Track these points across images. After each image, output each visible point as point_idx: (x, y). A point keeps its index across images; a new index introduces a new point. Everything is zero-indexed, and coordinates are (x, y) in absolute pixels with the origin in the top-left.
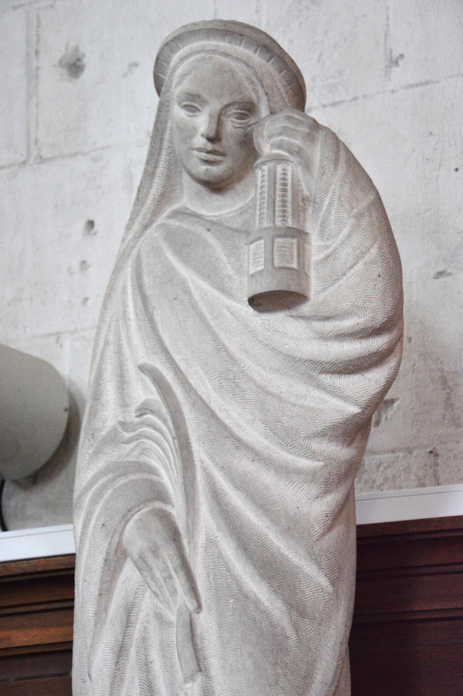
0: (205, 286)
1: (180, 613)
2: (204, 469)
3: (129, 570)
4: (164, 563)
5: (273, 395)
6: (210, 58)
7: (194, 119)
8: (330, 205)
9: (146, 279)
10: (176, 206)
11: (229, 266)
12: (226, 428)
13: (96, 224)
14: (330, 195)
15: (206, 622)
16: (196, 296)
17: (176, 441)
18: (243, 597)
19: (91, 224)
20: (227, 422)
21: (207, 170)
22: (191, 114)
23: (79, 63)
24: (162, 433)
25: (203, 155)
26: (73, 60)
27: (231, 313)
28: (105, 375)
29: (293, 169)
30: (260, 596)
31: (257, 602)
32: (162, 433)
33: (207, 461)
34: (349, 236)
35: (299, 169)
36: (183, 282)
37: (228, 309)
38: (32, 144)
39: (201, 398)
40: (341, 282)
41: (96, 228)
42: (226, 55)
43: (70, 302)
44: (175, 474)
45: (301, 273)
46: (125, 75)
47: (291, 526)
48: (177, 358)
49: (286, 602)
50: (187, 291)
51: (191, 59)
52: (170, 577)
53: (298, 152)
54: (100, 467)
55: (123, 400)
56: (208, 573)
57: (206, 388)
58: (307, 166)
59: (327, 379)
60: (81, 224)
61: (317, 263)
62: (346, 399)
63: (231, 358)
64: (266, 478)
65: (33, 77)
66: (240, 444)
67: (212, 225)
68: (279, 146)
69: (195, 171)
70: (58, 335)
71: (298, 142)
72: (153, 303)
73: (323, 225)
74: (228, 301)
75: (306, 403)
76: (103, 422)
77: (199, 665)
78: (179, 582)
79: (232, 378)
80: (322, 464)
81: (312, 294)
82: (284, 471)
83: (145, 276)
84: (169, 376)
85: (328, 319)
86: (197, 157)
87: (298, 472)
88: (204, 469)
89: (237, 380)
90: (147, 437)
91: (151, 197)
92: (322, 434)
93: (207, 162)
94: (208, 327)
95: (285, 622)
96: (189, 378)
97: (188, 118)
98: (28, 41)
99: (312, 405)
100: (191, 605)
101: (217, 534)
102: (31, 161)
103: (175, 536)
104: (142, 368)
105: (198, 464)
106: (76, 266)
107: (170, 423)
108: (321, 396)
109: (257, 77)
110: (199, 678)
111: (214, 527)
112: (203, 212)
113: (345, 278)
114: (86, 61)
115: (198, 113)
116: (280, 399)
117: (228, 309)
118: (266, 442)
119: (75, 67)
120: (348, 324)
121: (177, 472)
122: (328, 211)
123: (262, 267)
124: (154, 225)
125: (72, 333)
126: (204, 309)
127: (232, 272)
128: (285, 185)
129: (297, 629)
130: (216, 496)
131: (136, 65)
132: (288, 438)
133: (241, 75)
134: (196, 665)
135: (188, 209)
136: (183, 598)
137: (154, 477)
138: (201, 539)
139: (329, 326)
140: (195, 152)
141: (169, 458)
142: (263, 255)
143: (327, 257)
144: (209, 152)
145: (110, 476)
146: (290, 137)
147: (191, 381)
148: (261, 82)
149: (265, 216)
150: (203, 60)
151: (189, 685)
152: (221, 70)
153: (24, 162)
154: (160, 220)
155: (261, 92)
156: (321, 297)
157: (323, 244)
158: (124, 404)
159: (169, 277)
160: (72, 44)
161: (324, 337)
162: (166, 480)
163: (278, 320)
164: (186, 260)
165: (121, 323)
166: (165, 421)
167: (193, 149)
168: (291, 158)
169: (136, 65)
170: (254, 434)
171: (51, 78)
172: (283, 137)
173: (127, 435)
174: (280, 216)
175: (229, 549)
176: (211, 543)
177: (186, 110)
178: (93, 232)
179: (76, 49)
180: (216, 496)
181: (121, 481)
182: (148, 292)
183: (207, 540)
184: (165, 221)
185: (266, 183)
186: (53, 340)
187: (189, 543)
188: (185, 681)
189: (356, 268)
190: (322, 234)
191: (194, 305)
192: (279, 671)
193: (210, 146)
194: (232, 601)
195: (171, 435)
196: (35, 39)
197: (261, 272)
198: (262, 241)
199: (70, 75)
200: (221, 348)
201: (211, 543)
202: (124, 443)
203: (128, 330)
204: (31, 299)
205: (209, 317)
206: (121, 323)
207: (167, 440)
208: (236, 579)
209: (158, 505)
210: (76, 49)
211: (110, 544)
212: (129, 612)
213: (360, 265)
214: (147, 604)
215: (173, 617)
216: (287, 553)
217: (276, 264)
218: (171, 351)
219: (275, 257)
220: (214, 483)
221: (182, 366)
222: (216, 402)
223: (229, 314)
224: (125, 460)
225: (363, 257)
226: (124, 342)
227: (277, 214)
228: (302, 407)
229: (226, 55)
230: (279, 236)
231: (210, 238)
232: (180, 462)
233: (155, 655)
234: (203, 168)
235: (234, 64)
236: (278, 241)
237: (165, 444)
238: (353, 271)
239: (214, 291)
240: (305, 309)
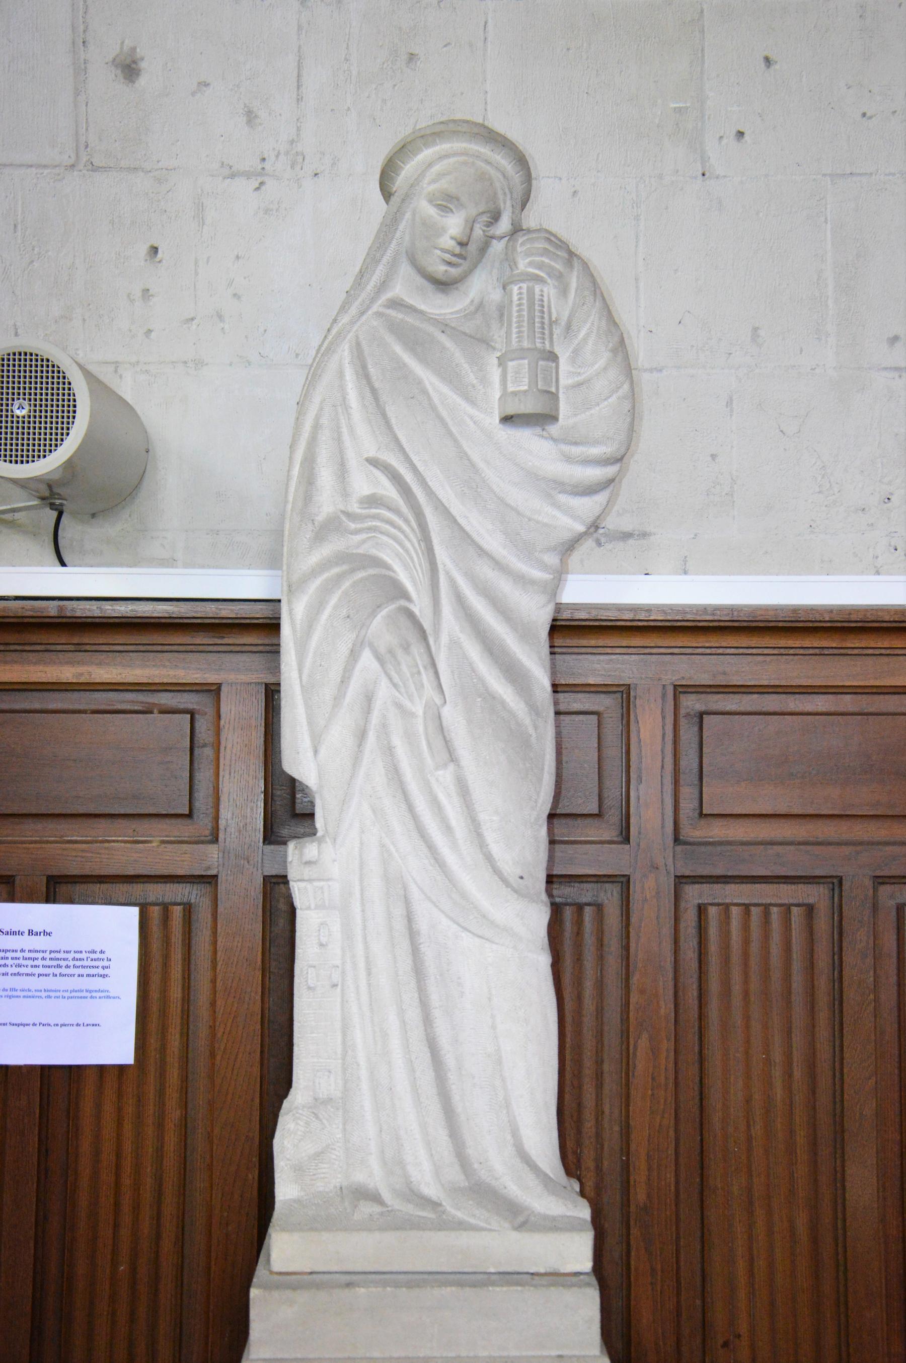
0: (445, 389)
1: (427, 706)
2: (447, 573)
3: (367, 658)
4: (415, 660)
5: (512, 508)
6: (473, 163)
7: (444, 219)
8: (588, 335)
9: (372, 370)
10: (389, 295)
11: (471, 374)
12: (467, 534)
13: (160, 251)
14: (588, 325)
15: (452, 715)
16: (436, 400)
17: (422, 544)
18: (490, 697)
19: (154, 250)
20: (468, 528)
21: (446, 271)
22: (443, 214)
23: (134, 66)
24: (403, 532)
25: (447, 257)
26: (128, 61)
27: (475, 423)
28: (319, 460)
29: (550, 291)
30: (505, 697)
31: (503, 703)
32: (403, 532)
33: (450, 565)
34: (605, 369)
35: (553, 292)
36: (420, 382)
37: (471, 418)
38: (82, 147)
39: (443, 505)
40: (593, 411)
41: (160, 255)
42: (488, 162)
43: (130, 331)
44: (421, 575)
45: (554, 397)
46: (193, 94)
47: (524, 632)
48: (415, 459)
49: (527, 703)
50: (424, 392)
51: (452, 160)
52: (419, 673)
53: (560, 277)
54: (325, 555)
55: (344, 489)
56: (452, 672)
57: (447, 494)
58: (564, 291)
59: (563, 498)
60: (144, 249)
61: (567, 388)
62: (575, 517)
63: (473, 465)
64: (505, 586)
65: (81, 70)
66: (482, 552)
67: (444, 327)
68: (540, 266)
69: (430, 269)
70: (116, 364)
71: (559, 266)
72: (384, 397)
73: (576, 352)
74: (470, 409)
75: (540, 518)
76: (319, 507)
77: (451, 756)
78: (426, 678)
79: (474, 485)
80: (552, 576)
81: (561, 417)
82: (521, 580)
83: (370, 366)
84: (409, 477)
85: (576, 444)
86: (439, 256)
87: (532, 582)
88: (447, 573)
89: (479, 490)
90: (381, 533)
91: (372, 284)
92: (549, 549)
93: (449, 264)
94: (450, 434)
95: (527, 721)
96: (428, 480)
97: (439, 218)
98: (74, 28)
99: (545, 520)
100: (438, 700)
101: (461, 635)
102: (81, 166)
103: (423, 635)
104: (373, 462)
105: (440, 567)
106: (138, 294)
107: (414, 524)
108: (553, 513)
109: (509, 189)
110: (451, 767)
111: (457, 628)
112: (423, 307)
113: (597, 408)
114: (143, 65)
115: (450, 214)
116: (518, 513)
117: (471, 418)
118: (504, 552)
119: (129, 69)
120: (595, 451)
121: (423, 574)
122: (585, 339)
123: (526, 388)
124: (370, 312)
125: (133, 365)
126: (444, 414)
127: (475, 382)
128: (543, 306)
129: (536, 728)
130: (460, 599)
131: (207, 85)
132: (527, 550)
133: (497, 185)
134: (448, 756)
135: (403, 300)
136: (429, 690)
137: (384, 572)
138: (444, 639)
139: (576, 450)
140: (438, 252)
141: (411, 558)
142: (527, 375)
143: (579, 385)
144: (455, 255)
145: (345, 567)
146: (550, 260)
147: (430, 483)
148: (511, 193)
149: (525, 334)
150: (465, 163)
151: (441, 772)
152: (482, 177)
153: (73, 166)
154: (375, 308)
155: (509, 203)
156: (571, 421)
157: (572, 369)
158: (345, 492)
159: (402, 373)
160: (128, 43)
161: (568, 459)
162: (403, 577)
163: (525, 436)
164: (423, 360)
165: (340, 409)
166: (406, 521)
167: (436, 248)
168: (549, 281)
169: (207, 85)
170: (494, 543)
171: (103, 79)
172: (543, 259)
173: (353, 526)
174: (539, 338)
175: (474, 652)
176: (454, 644)
177: (439, 209)
178: (157, 260)
179: (133, 50)
180: (460, 599)
181: (361, 574)
182: (377, 385)
183: (451, 640)
184: (381, 310)
185: (525, 301)
186: (111, 369)
187: (435, 641)
188: (437, 769)
189: (610, 400)
190: (573, 360)
191: (434, 408)
192: (528, 765)
193: (457, 250)
194: (479, 699)
195: (417, 537)
196: (82, 28)
197: (525, 392)
198: (526, 361)
199: (125, 78)
200: (463, 455)
201: (454, 644)
202: (351, 534)
203: (349, 419)
204: (84, 320)
205: (450, 423)
206: (340, 409)
207: (409, 540)
208: (482, 680)
209: (403, 603)
210: (133, 50)
211: (357, 637)
212: (369, 699)
213: (614, 397)
214: (384, 691)
215: (419, 710)
216: (521, 657)
217: (539, 387)
218: (407, 450)
219: (539, 380)
220: (457, 587)
221: (421, 468)
222: (456, 508)
223: (471, 423)
224: (354, 551)
225: (617, 391)
226: (345, 430)
227: (537, 335)
228: (538, 522)
229: (488, 162)
230: (543, 359)
231: (443, 339)
232: (428, 565)
233: (397, 741)
234: (443, 268)
235: (492, 172)
236: (541, 363)
237: (408, 545)
238: (606, 403)
239: (455, 396)
240: (554, 429)
